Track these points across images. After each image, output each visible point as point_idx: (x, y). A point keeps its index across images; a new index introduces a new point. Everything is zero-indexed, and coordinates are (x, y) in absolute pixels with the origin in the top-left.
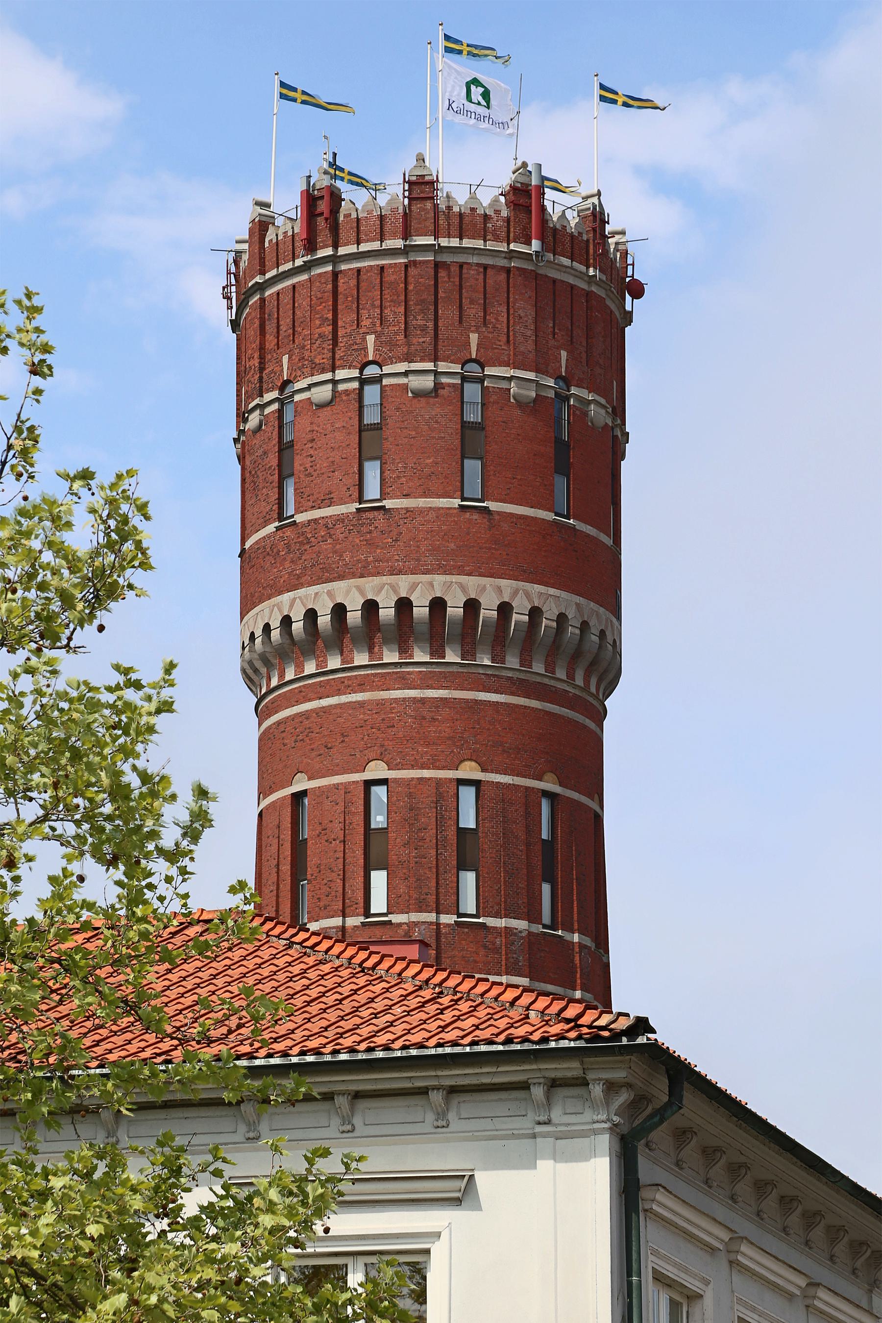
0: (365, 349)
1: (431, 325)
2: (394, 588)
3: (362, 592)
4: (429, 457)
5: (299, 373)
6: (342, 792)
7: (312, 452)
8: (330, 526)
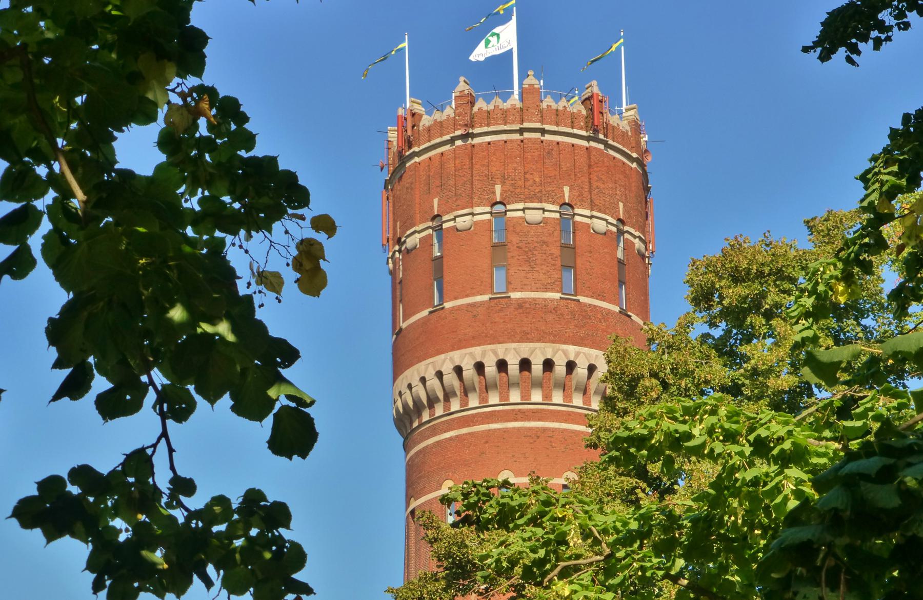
0: (494, 193)
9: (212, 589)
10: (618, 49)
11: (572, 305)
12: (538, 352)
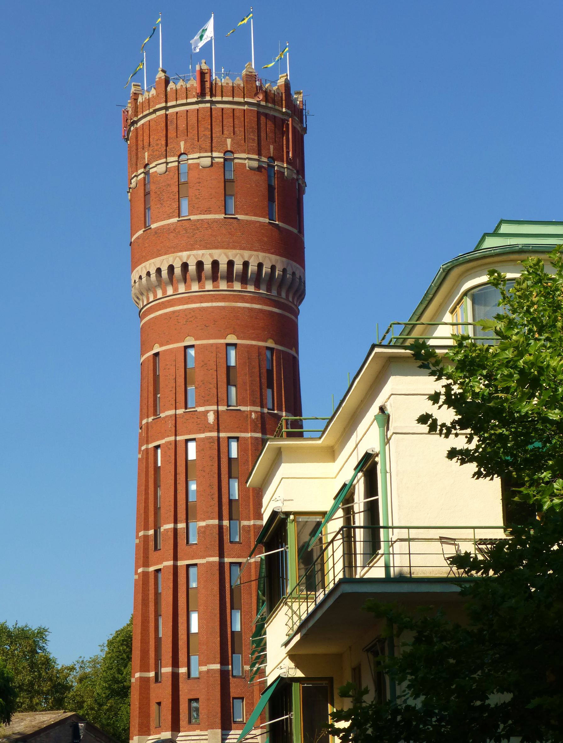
0: (227, 145)
1: (256, 138)
2: (242, 256)
3: (227, 256)
4: (256, 198)
5: (191, 151)
6: (215, 348)
7: (199, 188)
8: (210, 223)
9: (380, 404)
10: (249, 22)
11: (186, 224)
12: (165, 261)
